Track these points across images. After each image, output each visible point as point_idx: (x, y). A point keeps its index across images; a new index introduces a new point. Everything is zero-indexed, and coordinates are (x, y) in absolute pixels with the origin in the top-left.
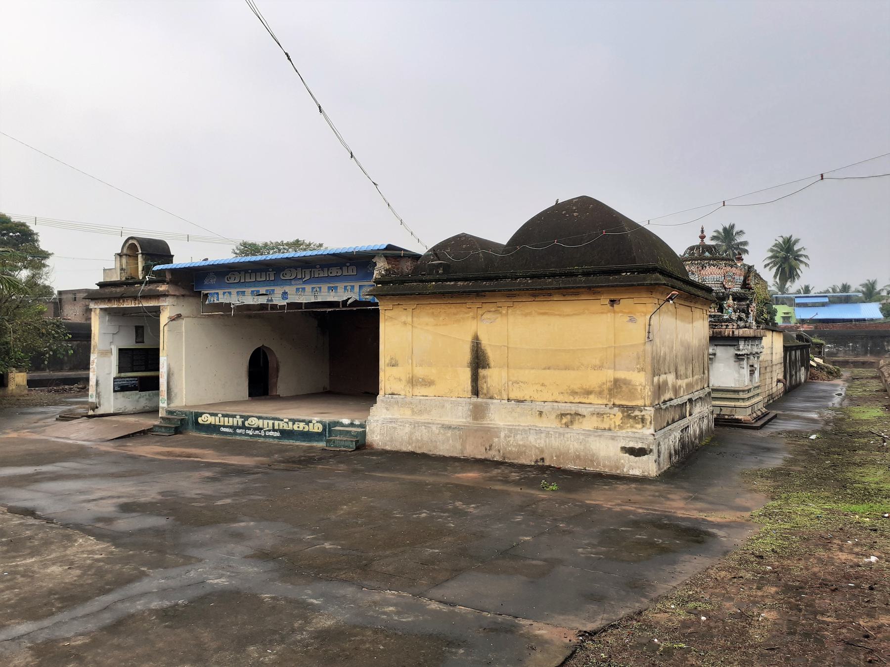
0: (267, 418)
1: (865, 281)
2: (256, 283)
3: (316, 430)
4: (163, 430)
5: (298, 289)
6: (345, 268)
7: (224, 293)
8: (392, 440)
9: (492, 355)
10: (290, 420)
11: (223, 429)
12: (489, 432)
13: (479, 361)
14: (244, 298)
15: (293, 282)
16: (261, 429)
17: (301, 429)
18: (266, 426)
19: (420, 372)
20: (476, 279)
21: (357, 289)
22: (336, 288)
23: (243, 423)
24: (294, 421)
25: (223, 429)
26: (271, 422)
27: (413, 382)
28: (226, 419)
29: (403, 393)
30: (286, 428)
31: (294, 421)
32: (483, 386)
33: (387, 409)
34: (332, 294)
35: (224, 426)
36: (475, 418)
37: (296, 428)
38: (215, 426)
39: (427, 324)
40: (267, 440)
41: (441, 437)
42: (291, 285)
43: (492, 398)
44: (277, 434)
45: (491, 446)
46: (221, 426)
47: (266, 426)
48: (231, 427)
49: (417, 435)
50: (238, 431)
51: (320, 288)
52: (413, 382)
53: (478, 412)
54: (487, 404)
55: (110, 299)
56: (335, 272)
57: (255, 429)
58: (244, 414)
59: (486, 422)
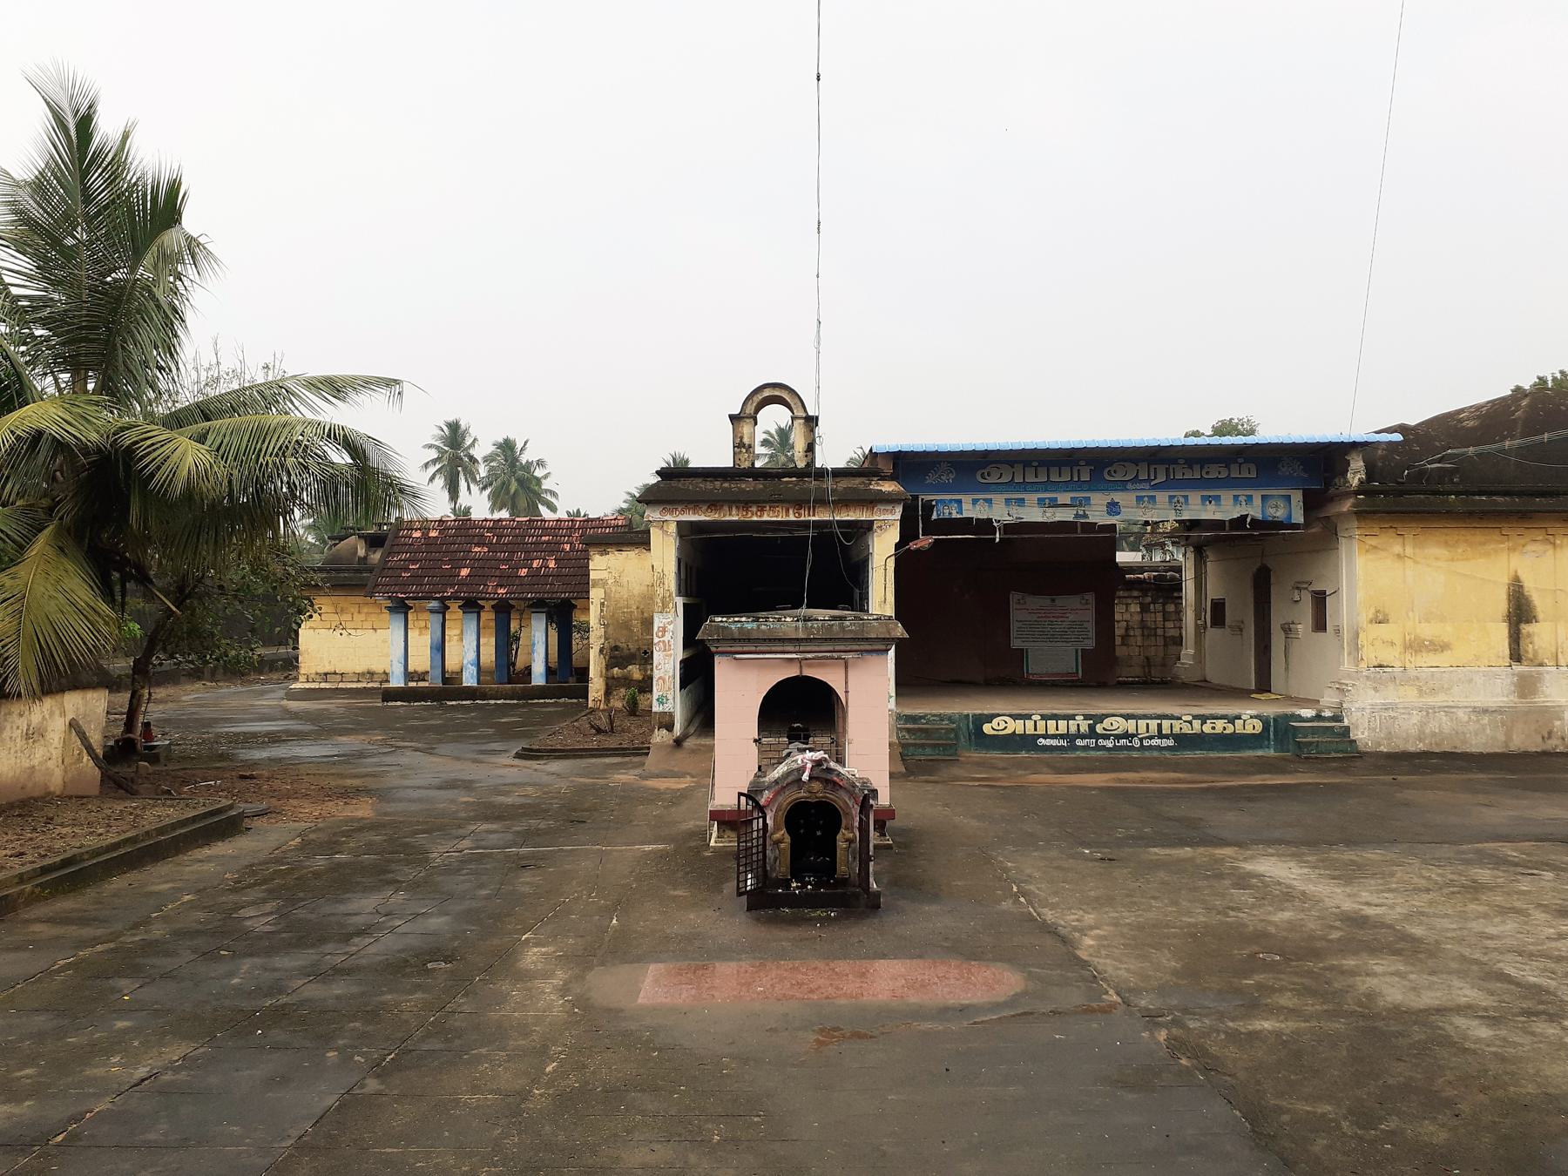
0: (1145, 717)
1: (451, 419)
2: (1049, 485)
3: (1249, 730)
4: (928, 751)
5: (1139, 499)
6: (1234, 467)
7: (975, 502)
8: (1389, 736)
9: (1539, 602)
10: (1195, 717)
11: (1042, 742)
12: (1548, 714)
13: (1520, 612)
14: (1021, 510)
15: (1129, 486)
16: (1133, 736)
17: (1219, 730)
18: (1142, 729)
19: (1427, 631)
20: (1520, 494)
21: (1257, 501)
22: (1218, 498)
23: (1092, 728)
24: (1204, 719)
25: (1042, 742)
26: (1153, 724)
27: (1416, 646)
28: (1051, 723)
29: (1397, 664)
30: (1187, 729)
31: (1204, 719)
32: (1528, 649)
33: (1375, 689)
34: (1211, 507)
35: (1046, 736)
36: (1522, 695)
37: (1207, 729)
38: (1024, 736)
39: (1437, 559)
40: (1147, 754)
41: (1472, 727)
42: (1125, 489)
43: (1541, 665)
44: (1171, 742)
45: (1550, 733)
46: (1040, 736)
47: (1142, 729)
48: (1062, 736)
49: (1433, 726)
50: (1079, 742)
51: (1186, 497)
52: (1416, 646)
53: (1526, 686)
54: (1539, 673)
55: (692, 502)
56: (1214, 472)
57: (1118, 737)
58: (1093, 712)
59: (1539, 700)
